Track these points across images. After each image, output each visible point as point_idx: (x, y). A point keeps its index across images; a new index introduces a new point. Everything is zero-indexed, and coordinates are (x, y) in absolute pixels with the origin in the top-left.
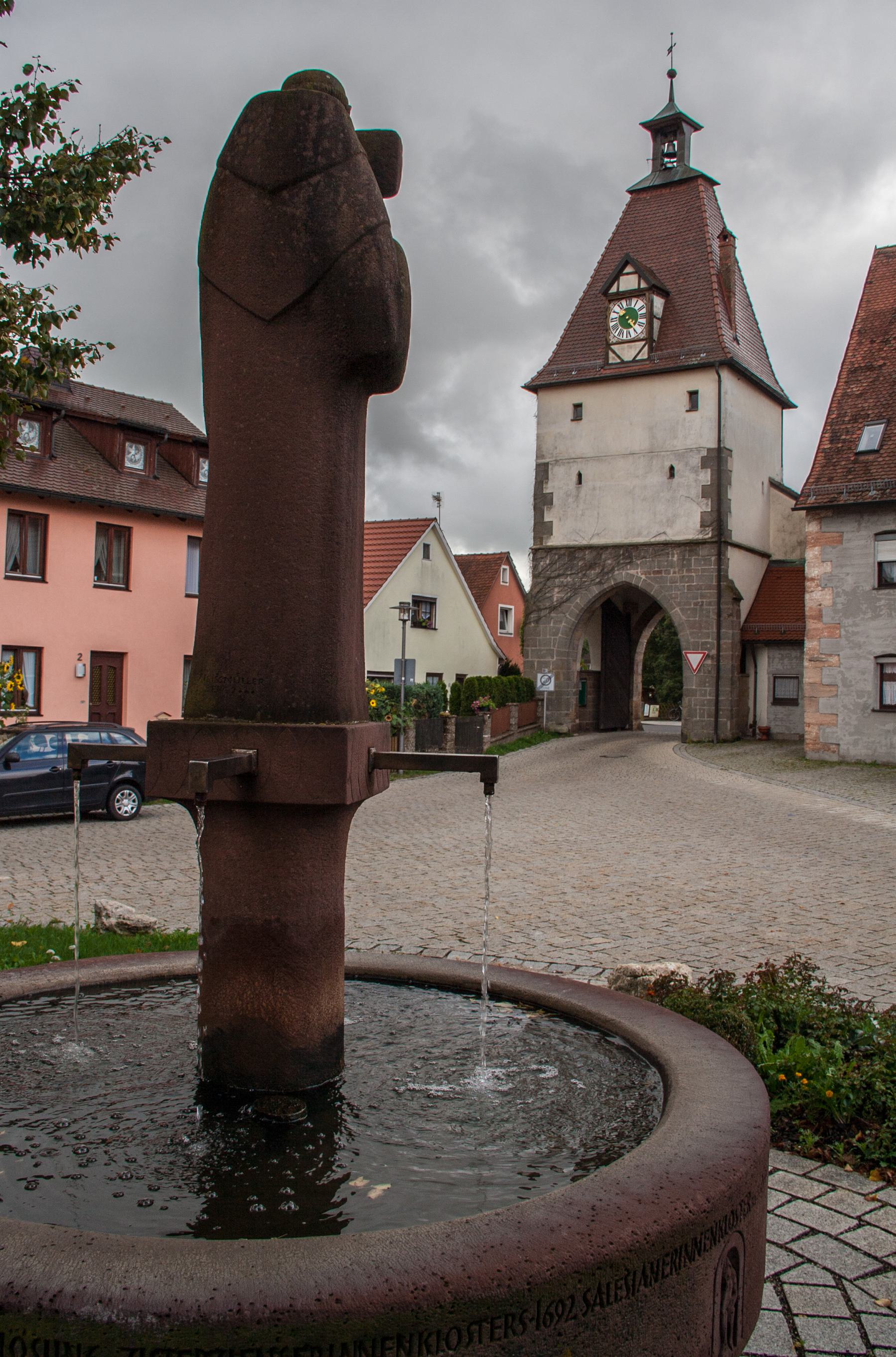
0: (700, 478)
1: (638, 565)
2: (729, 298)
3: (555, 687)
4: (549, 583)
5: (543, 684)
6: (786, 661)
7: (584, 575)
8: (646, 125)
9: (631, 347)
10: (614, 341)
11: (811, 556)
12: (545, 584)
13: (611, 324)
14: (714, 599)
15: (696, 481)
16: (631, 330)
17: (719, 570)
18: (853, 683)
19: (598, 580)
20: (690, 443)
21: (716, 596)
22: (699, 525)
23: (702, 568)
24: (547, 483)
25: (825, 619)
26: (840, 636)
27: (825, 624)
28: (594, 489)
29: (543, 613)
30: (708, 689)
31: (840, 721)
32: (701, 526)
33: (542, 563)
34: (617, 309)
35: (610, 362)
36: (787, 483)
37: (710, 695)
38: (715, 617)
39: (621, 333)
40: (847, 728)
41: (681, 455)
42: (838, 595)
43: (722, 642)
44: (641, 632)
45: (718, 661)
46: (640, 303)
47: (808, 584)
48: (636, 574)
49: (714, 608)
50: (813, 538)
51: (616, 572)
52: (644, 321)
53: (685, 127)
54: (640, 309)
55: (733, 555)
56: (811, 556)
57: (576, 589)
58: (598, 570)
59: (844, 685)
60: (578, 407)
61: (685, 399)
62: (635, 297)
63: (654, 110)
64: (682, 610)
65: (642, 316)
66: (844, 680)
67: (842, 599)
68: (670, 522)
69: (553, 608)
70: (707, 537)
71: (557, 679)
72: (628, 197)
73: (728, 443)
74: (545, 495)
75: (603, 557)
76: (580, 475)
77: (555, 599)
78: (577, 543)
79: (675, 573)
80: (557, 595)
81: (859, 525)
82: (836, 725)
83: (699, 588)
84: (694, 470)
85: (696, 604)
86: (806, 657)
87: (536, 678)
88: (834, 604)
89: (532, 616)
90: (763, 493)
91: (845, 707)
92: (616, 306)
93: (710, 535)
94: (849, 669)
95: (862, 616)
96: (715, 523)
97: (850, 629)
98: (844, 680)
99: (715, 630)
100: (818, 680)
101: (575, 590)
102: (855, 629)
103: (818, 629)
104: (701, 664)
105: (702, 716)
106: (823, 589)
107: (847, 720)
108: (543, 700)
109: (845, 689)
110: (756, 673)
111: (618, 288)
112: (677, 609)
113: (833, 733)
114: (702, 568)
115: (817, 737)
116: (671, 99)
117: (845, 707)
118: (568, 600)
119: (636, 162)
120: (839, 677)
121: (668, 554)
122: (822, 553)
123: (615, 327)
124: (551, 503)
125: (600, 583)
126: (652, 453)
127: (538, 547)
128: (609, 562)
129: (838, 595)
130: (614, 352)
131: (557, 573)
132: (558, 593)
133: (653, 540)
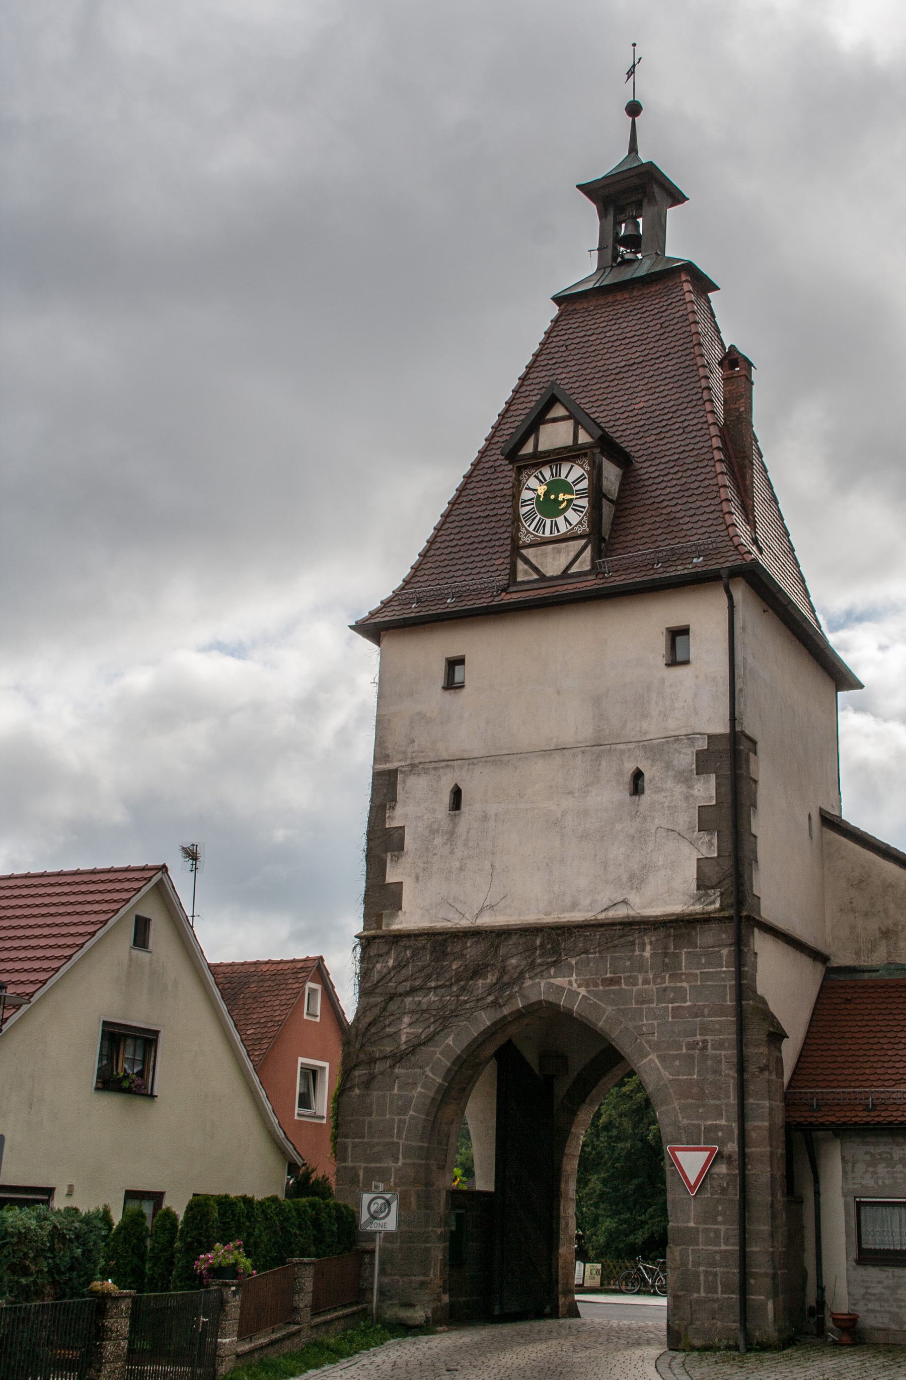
0: (695, 792)
6: (881, 1169)
9: (559, 552)
13: (523, 510)
15: (687, 798)
16: (560, 520)
21: (734, 1028)
38: (733, 1073)
39: (541, 525)
43: (750, 1125)
52: (584, 502)
104: (706, 1175)
105: (711, 1289)
110: (817, 1193)
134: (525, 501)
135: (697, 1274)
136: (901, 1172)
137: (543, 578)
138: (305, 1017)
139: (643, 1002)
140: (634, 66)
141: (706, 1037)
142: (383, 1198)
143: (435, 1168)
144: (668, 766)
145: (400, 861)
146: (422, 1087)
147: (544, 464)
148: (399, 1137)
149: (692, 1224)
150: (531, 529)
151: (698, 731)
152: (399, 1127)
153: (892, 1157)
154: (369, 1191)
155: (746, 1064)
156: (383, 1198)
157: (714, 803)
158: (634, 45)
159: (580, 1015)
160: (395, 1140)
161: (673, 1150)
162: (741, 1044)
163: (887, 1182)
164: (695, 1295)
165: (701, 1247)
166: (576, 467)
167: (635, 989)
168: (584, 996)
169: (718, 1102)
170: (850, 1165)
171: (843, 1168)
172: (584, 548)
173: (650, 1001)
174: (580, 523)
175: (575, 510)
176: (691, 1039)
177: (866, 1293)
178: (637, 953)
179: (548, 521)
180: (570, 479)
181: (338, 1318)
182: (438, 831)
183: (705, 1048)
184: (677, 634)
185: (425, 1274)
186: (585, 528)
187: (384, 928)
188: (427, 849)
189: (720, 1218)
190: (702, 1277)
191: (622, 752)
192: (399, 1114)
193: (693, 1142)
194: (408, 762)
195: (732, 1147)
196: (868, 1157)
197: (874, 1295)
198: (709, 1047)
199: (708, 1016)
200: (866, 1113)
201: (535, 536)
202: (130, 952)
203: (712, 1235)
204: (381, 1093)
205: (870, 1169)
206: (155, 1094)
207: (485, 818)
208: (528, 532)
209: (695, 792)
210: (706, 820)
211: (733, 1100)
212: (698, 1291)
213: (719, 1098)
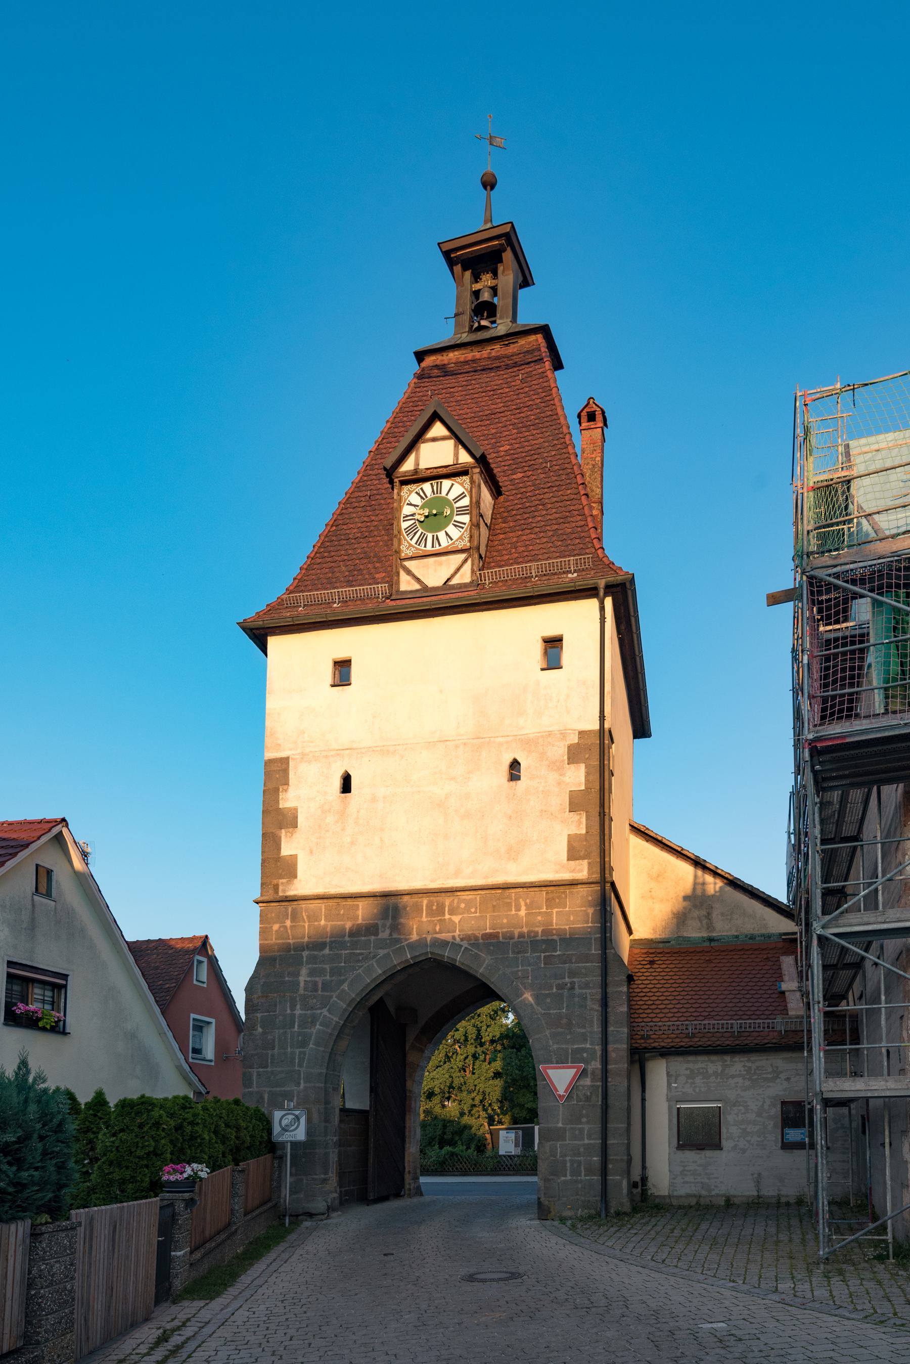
0: (567, 779)
3: (309, 1133)
6: (698, 1080)
9: (440, 564)
10: (410, 553)
13: (404, 525)
15: (559, 784)
16: (441, 535)
21: (598, 972)
37: (589, 1138)
38: (597, 1007)
39: (422, 539)
43: (610, 1047)
46: (458, 489)
54: (457, 499)
61: (538, 648)
104: (573, 1088)
105: (576, 1172)
110: (643, 1100)
111: (417, 463)
134: (407, 516)
135: (564, 1162)
136: (714, 1082)
137: (425, 588)
138: (195, 982)
139: (518, 953)
141: (574, 980)
142: (293, 1114)
143: (331, 1090)
144: (543, 755)
145: (294, 836)
146: (320, 1025)
148: (300, 1065)
149: (560, 1125)
151: (569, 727)
152: (299, 1058)
153: (707, 1072)
154: (282, 1108)
155: (608, 1000)
156: (293, 1114)
157: (583, 788)
159: (463, 964)
160: (297, 1068)
161: (545, 1069)
162: (605, 985)
163: (703, 1090)
164: (563, 1178)
165: (567, 1142)
166: (456, 486)
168: (466, 948)
169: (584, 1030)
170: (673, 1078)
171: (668, 1081)
172: (465, 561)
173: (525, 952)
174: (460, 538)
175: (455, 526)
176: (560, 981)
177: (684, 1170)
178: (513, 912)
179: (430, 536)
180: (451, 497)
181: (261, 1214)
182: (329, 811)
183: (572, 988)
184: (553, 644)
185: (326, 1173)
187: (281, 894)
188: (320, 826)
189: (584, 1120)
190: (568, 1165)
191: (501, 744)
192: (300, 1047)
193: (562, 1061)
194: (299, 751)
195: (596, 1065)
196: (688, 1072)
197: (690, 1171)
198: (576, 986)
199: (576, 963)
200: (687, 1040)
201: (417, 549)
202: (33, 900)
203: (577, 1132)
204: (282, 1031)
205: (690, 1081)
206: (67, 1031)
207: (374, 799)
208: (410, 545)
209: (567, 779)
210: (575, 803)
211: (597, 1028)
212: (566, 1176)
213: (584, 1027)
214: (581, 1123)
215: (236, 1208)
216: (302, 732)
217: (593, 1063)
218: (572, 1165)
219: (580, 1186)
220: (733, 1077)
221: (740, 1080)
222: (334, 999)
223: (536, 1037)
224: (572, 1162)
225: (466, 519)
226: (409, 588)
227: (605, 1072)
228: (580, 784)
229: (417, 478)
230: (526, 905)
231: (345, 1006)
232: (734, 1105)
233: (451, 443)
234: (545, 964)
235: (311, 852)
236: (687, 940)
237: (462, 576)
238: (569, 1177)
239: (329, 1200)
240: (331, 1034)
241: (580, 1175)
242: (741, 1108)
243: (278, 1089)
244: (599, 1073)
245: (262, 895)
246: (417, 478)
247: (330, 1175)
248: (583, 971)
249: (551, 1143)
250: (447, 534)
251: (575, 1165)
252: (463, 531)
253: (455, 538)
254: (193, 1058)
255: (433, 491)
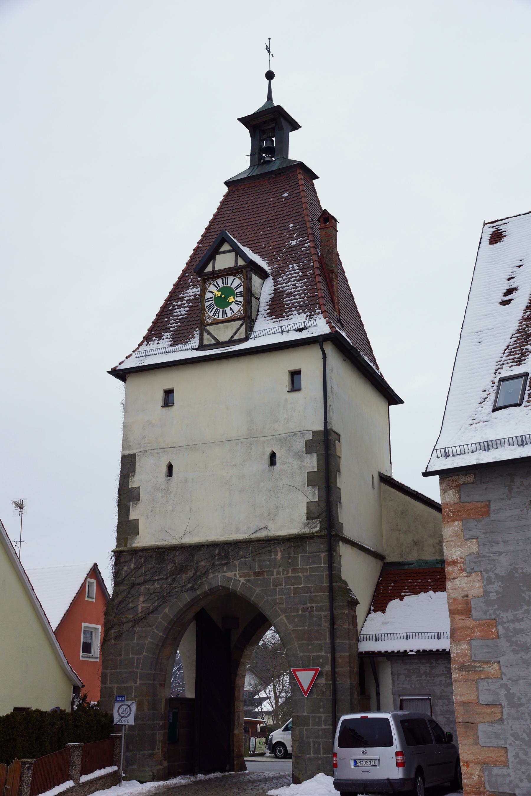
0: (305, 464)
1: (235, 566)
2: (331, 280)
3: (137, 718)
4: (133, 592)
5: (121, 716)
6: (414, 678)
7: (174, 580)
8: (245, 121)
9: (227, 327)
10: (209, 321)
11: (450, 533)
12: (129, 593)
13: (207, 304)
14: (326, 604)
15: (300, 467)
16: (228, 310)
17: (331, 569)
18: (524, 700)
19: (190, 585)
20: (293, 427)
21: (327, 599)
22: (305, 517)
23: (310, 567)
24: (133, 476)
25: (474, 614)
26: (498, 637)
27: (476, 620)
28: (186, 481)
29: (125, 627)
30: (323, 715)
31: (511, 759)
32: (308, 519)
33: (125, 568)
34: (212, 288)
35: (204, 344)
36: (397, 476)
37: (325, 724)
38: (328, 625)
39: (217, 312)
40: (523, 768)
41: (284, 440)
42: (489, 581)
43: (337, 655)
44: (242, 651)
45: (334, 679)
46: (237, 282)
47: (448, 569)
48: (233, 577)
49: (325, 613)
50: (450, 511)
51: (211, 576)
52: (241, 299)
53: (284, 123)
54: (237, 287)
55: (345, 552)
56: (450, 533)
57: (164, 597)
58: (190, 574)
59: (512, 704)
60: (169, 393)
61: (286, 379)
62: (231, 275)
63: (254, 104)
64: (288, 617)
65: (239, 294)
66: (510, 697)
67: (496, 586)
68: (272, 515)
69: (137, 621)
70: (314, 530)
71: (139, 709)
72: (225, 190)
73: (335, 425)
74: (131, 490)
75: (196, 558)
76: (170, 467)
77: (140, 610)
78: (165, 543)
79: (278, 573)
80: (141, 605)
81: (510, 490)
82: (506, 764)
83: (307, 590)
84: (299, 456)
85: (304, 610)
86: (454, 666)
87: (112, 709)
88: (486, 593)
89: (113, 631)
90: (373, 487)
91: (515, 735)
92: (212, 286)
93: (318, 528)
94: (516, 681)
95: (526, 607)
96: (324, 514)
97: (511, 626)
98: (510, 697)
99: (328, 641)
100: (472, 697)
101: (163, 598)
102: (517, 625)
103: (467, 628)
104: (313, 684)
105: (317, 752)
106: (469, 574)
107: (521, 755)
108: (121, 737)
109: (513, 711)
110: (378, 694)
111: (214, 267)
112: (283, 617)
113: (504, 776)
114: (310, 567)
115: (481, 783)
116: (270, 98)
117: (515, 735)
118: (155, 610)
119: (236, 155)
120: (503, 693)
121: (271, 552)
122: (464, 529)
123: (210, 307)
124: (138, 499)
125: (192, 589)
126: (251, 438)
127: (122, 549)
128: (203, 563)
129: (489, 581)
130: (209, 333)
131: (142, 579)
132: (144, 602)
133: (253, 536)
134: (208, 299)
135: (309, 743)
138: (87, 599)
139: (276, 586)
140: (270, 53)
146: (151, 639)
147: (218, 277)
149: (306, 714)
150: (211, 315)
152: (137, 662)
157: (316, 470)
158: (270, 39)
159: (241, 594)
162: (332, 608)
163: (417, 686)
164: (308, 756)
165: (310, 727)
167: (272, 577)
169: (320, 642)
174: (239, 311)
178: (273, 557)
179: (221, 310)
180: (233, 286)
183: (312, 611)
184: (295, 374)
185: (153, 749)
186: (242, 314)
189: (321, 710)
190: (312, 745)
195: (328, 668)
196: (406, 672)
199: (314, 592)
201: (214, 319)
203: (317, 720)
205: (408, 679)
208: (210, 316)
209: (305, 464)
212: (310, 754)
213: (320, 640)
214: (319, 713)
215: (74, 773)
216: (145, 437)
217: (327, 667)
218: (314, 745)
219: (320, 762)
220: (438, 676)
221: (443, 678)
222: (160, 619)
223: (289, 647)
224: (314, 742)
225: (241, 299)
226: (209, 343)
227: (334, 672)
228: (314, 467)
229: (215, 275)
230: (281, 551)
231: (166, 624)
232: (440, 699)
233: (233, 255)
234: (294, 594)
235: (147, 517)
236: (425, 562)
237: (240, 334)
238: (312, 755)
239: (155, 771)
240: (157, 645)
241: (320, 754)
242: (445, 701)
243: (123, 685)
244: (330, 673)
245: (117, 547)
246: (215, 275)
247: (157, 750)
248: (319, 598)
249: (300, 727)
250: (231, 309)
251: (316, 745)
252: (240, 306)
253: (236, 311)
254: (82, 657)
255: (223, 283)
